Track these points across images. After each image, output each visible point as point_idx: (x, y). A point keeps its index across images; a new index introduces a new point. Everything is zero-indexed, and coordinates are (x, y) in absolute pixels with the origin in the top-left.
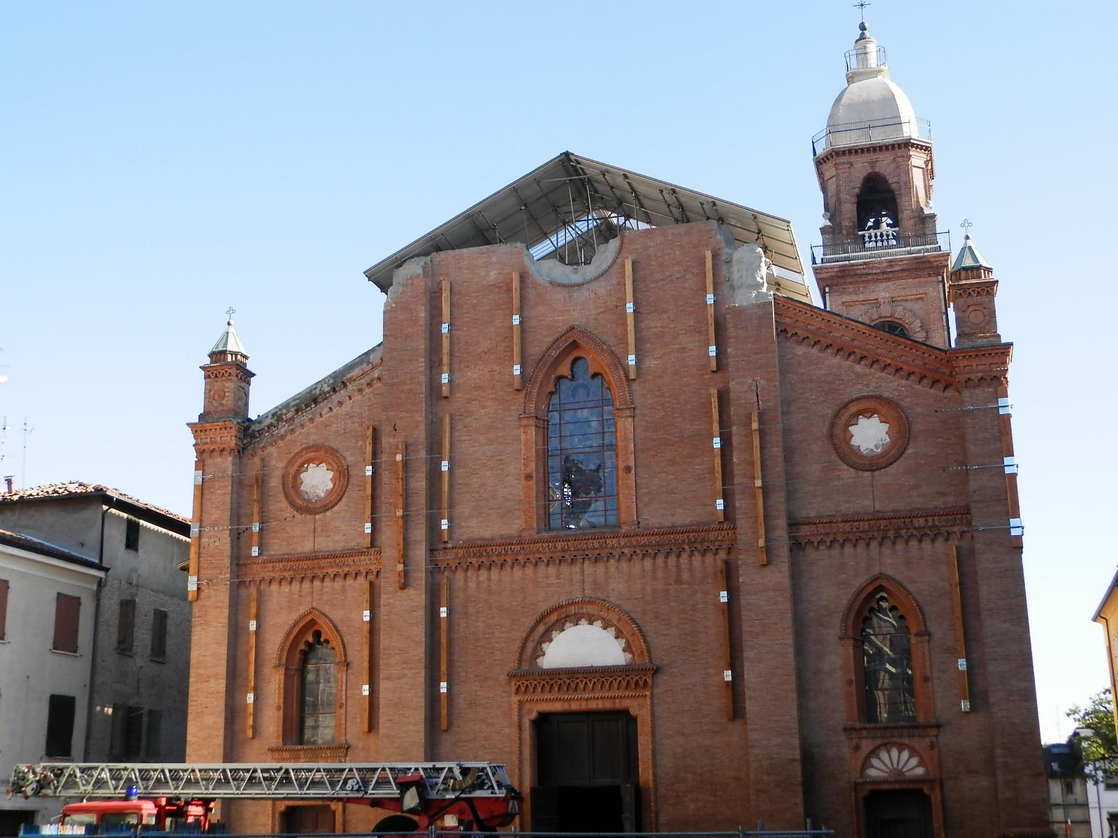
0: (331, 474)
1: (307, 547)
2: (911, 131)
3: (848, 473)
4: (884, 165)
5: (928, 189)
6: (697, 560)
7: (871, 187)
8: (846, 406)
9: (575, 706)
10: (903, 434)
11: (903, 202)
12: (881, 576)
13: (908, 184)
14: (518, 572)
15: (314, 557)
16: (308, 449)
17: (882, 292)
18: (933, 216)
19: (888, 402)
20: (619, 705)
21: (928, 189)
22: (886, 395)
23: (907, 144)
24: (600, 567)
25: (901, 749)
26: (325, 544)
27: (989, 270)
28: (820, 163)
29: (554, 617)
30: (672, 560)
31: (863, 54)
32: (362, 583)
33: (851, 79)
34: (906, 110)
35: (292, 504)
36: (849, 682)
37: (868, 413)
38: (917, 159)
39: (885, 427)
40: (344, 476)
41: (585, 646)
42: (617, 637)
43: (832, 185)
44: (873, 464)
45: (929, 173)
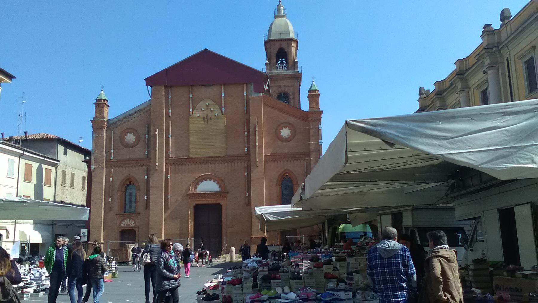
0: (134, 137)
1: (128, 157)
2: (292, 36)
3: (280, 143)
4: (284, 45)
5: (296, 53)
6: (239, 164)
7: (280, 50)
8: (280, 125)
9: (205, 202)
10: (294, 133)
11: (289, 57)
12: (287, 169)
13: (291, 52)
15: (130, 160)
16: (128, 129)
17: (282, 83)
18: (297, 62)
19: (290, 124)
20: (217, 202)
21: (296, 53)
22: (290, 122)
23: (291, 40)
25: (130, 219)
26: (132, 157)
27: (318, 91)
28: (266, 43)
29: (200, 178)
30: (233, 164)
31: (279, 10)
32: (144, 168)
33: (276, 17)
34: (291, 28)
35: (123, 145)
36: (278, 196)
37: (285, 127)
38: (294, 45)
39: (290, 131)
40: (138, 138)
41: (209, 186)
43: (269, 50)
44: (286, 140)
45: (297, 48)
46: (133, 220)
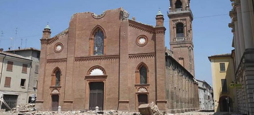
24: (100, 60)
42: (92, 71)
44: (143, 45)
46: (58, 90)
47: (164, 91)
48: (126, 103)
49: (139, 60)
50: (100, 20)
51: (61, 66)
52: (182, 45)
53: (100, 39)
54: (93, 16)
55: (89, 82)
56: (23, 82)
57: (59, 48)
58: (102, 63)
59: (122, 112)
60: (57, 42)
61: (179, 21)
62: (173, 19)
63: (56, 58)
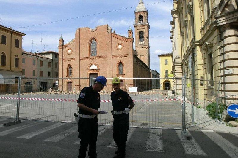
14: (88, 60)
41: (94, 67)
44: (120, 50)
47: (6, 111)
48: (5, 59)
49: (139, 14)
50: (94, 32)
51: (72, 63)
52: (142, 46)
53: (94, 45)
54: (90, 30)
55: (89, 73)
56: (49, 73)
57: (70, 51)
58: (97, 61)
59: (150, 150)
60: (67, 47)
61: (141, 30)
62: (137, 29)
63: (69, 58)
